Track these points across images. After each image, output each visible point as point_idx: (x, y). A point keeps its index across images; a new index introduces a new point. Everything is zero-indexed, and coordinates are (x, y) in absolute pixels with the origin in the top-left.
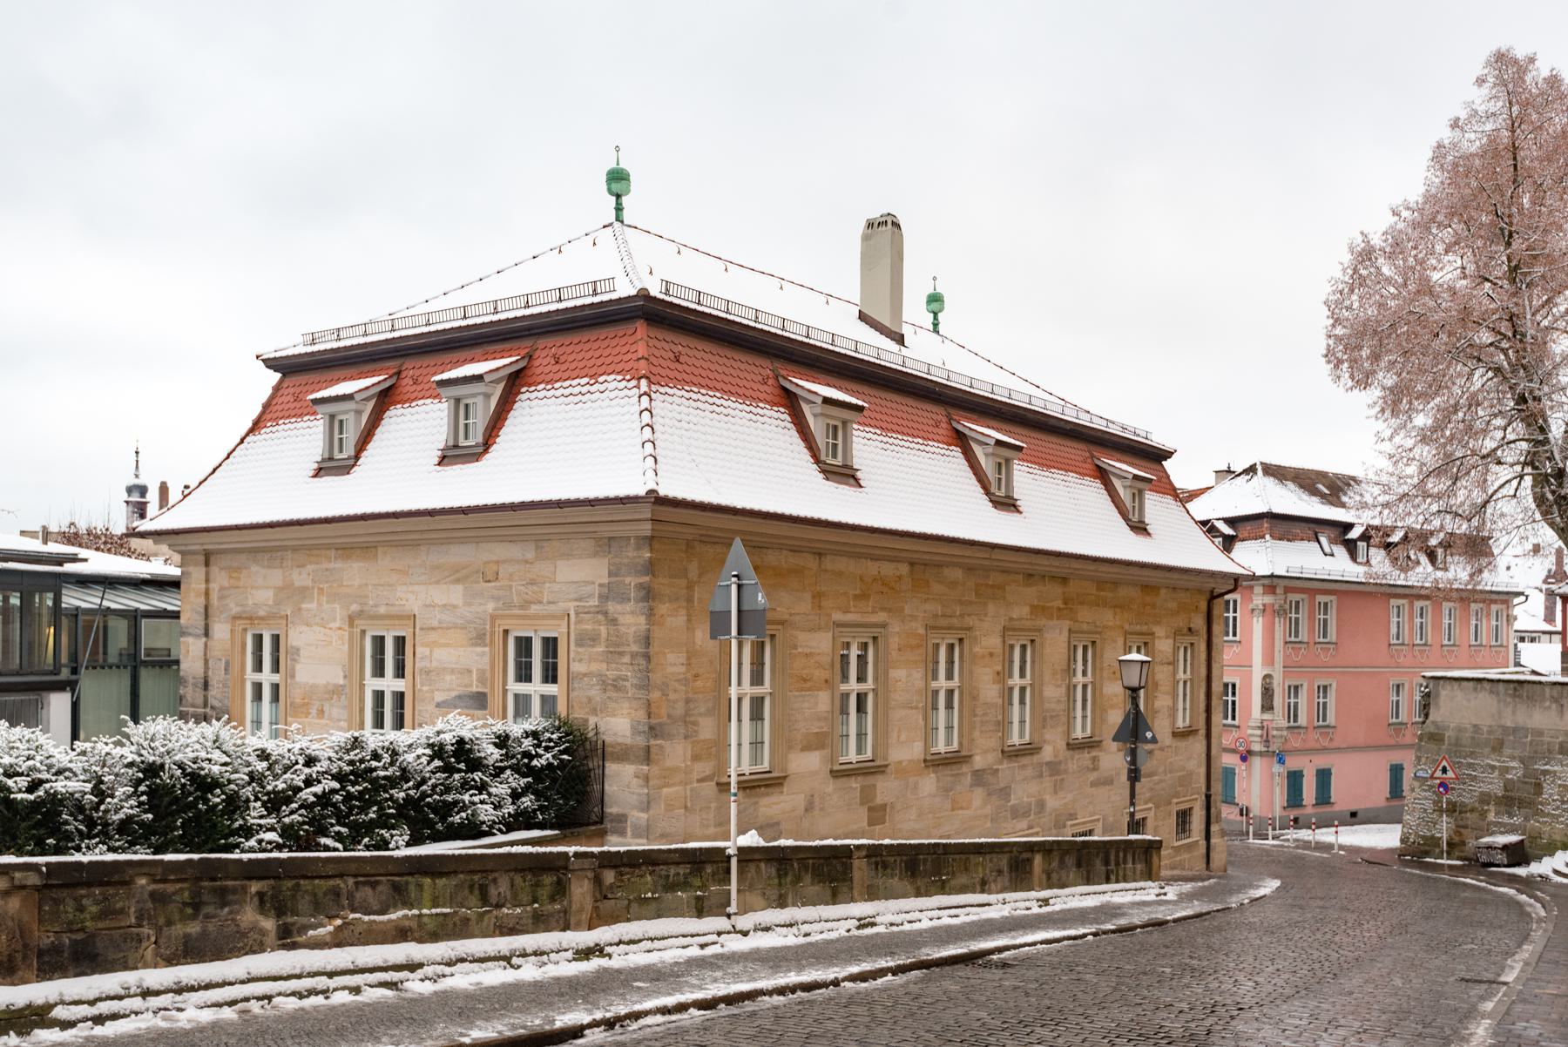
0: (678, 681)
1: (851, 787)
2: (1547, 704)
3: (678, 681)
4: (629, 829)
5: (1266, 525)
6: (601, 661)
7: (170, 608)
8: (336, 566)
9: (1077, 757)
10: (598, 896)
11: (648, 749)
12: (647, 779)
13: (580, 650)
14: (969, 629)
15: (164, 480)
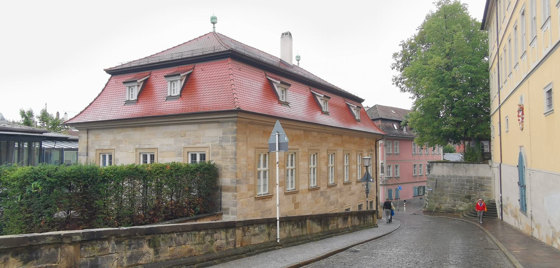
0: (244, 166)
1: (290, 198)
2: (462, 169)
3: (244, 166)
4: (230, 213)
5: (380, 121)
6: (220, 161)
7: (73, 147)
8: (131, 133)
9: (345, 187)
10: (243, 235)
11: (236, 187)
12: (236, 197)
13: (213, 157)
14: (319, 150)
15: (58, 111)
